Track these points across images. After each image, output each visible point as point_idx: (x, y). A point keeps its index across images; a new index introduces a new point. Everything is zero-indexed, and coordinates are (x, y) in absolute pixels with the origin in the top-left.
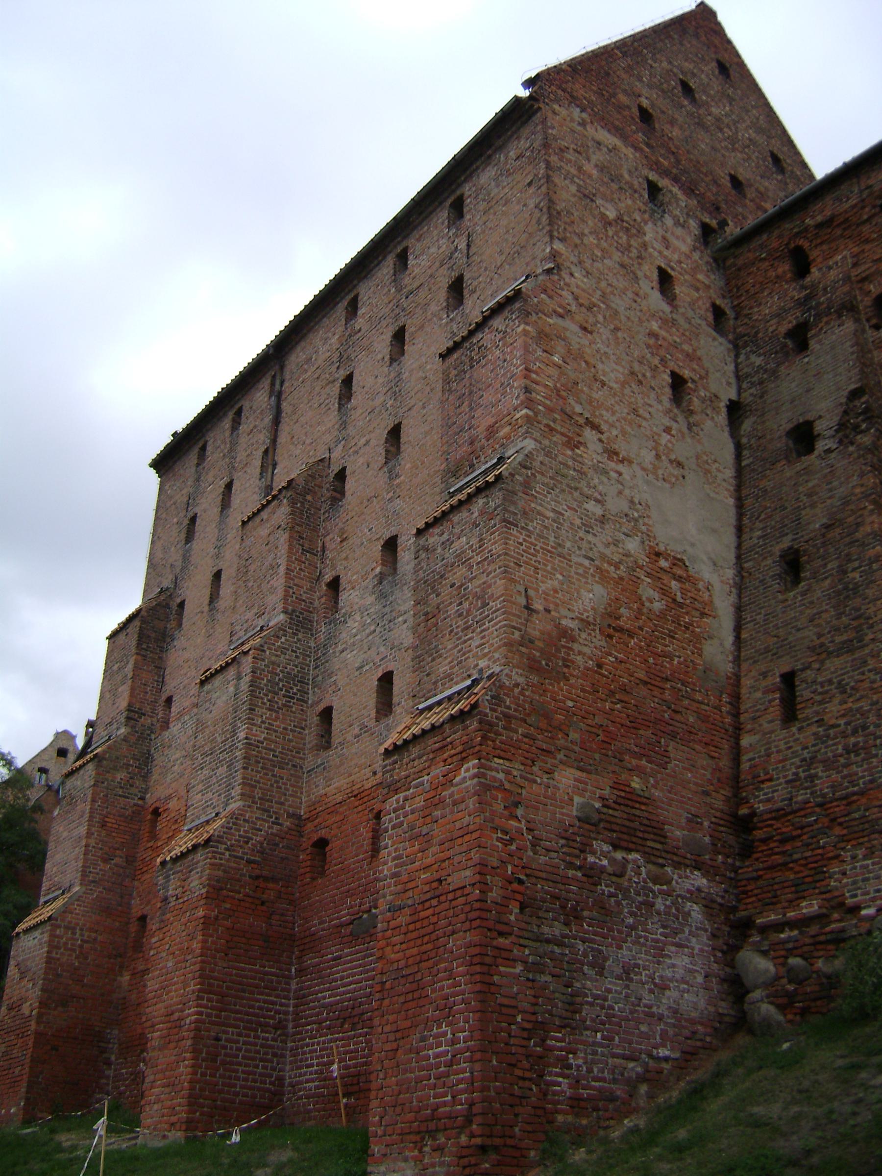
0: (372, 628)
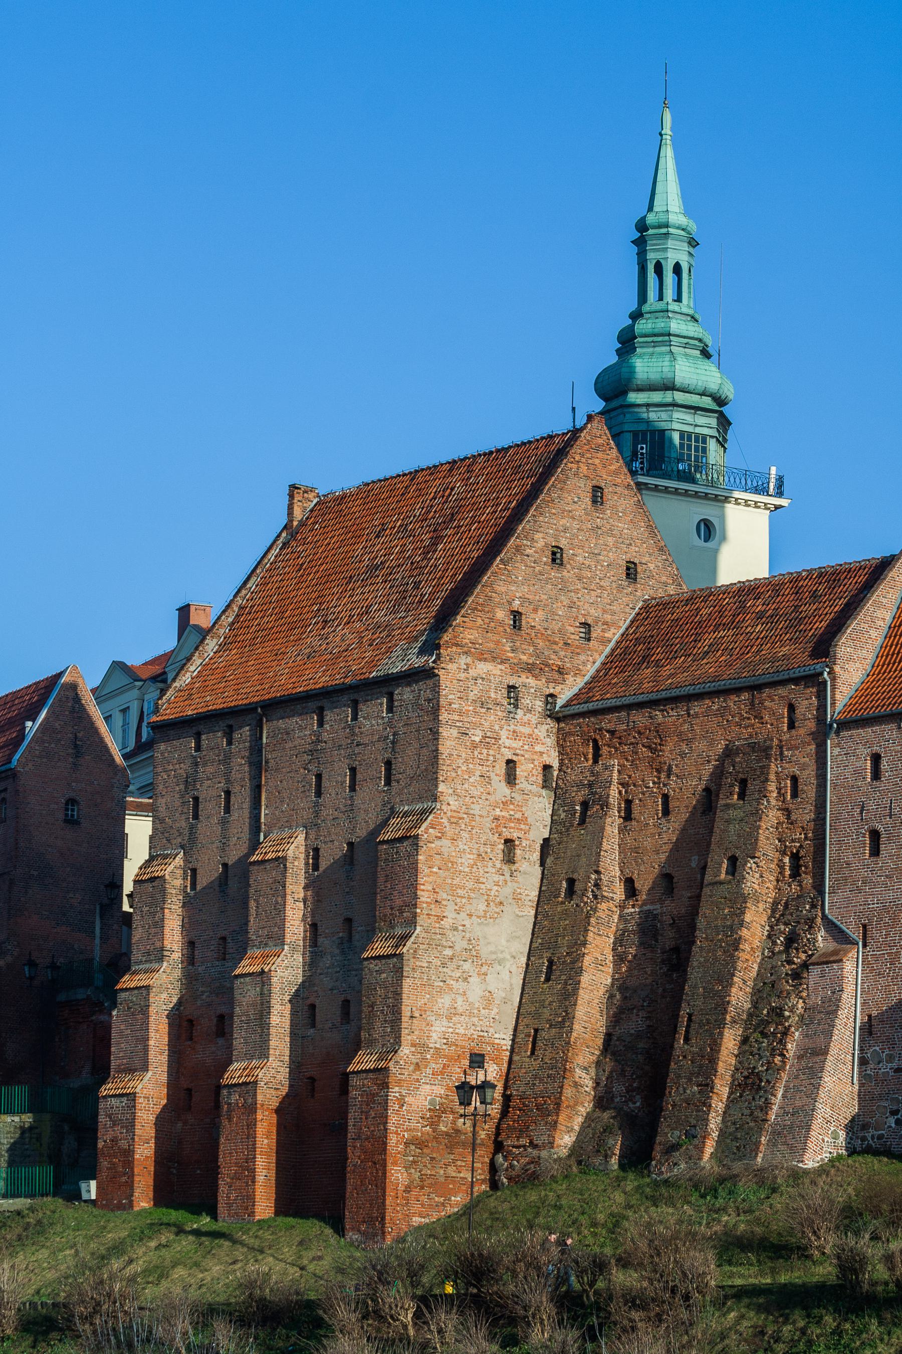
0: (338, 969)
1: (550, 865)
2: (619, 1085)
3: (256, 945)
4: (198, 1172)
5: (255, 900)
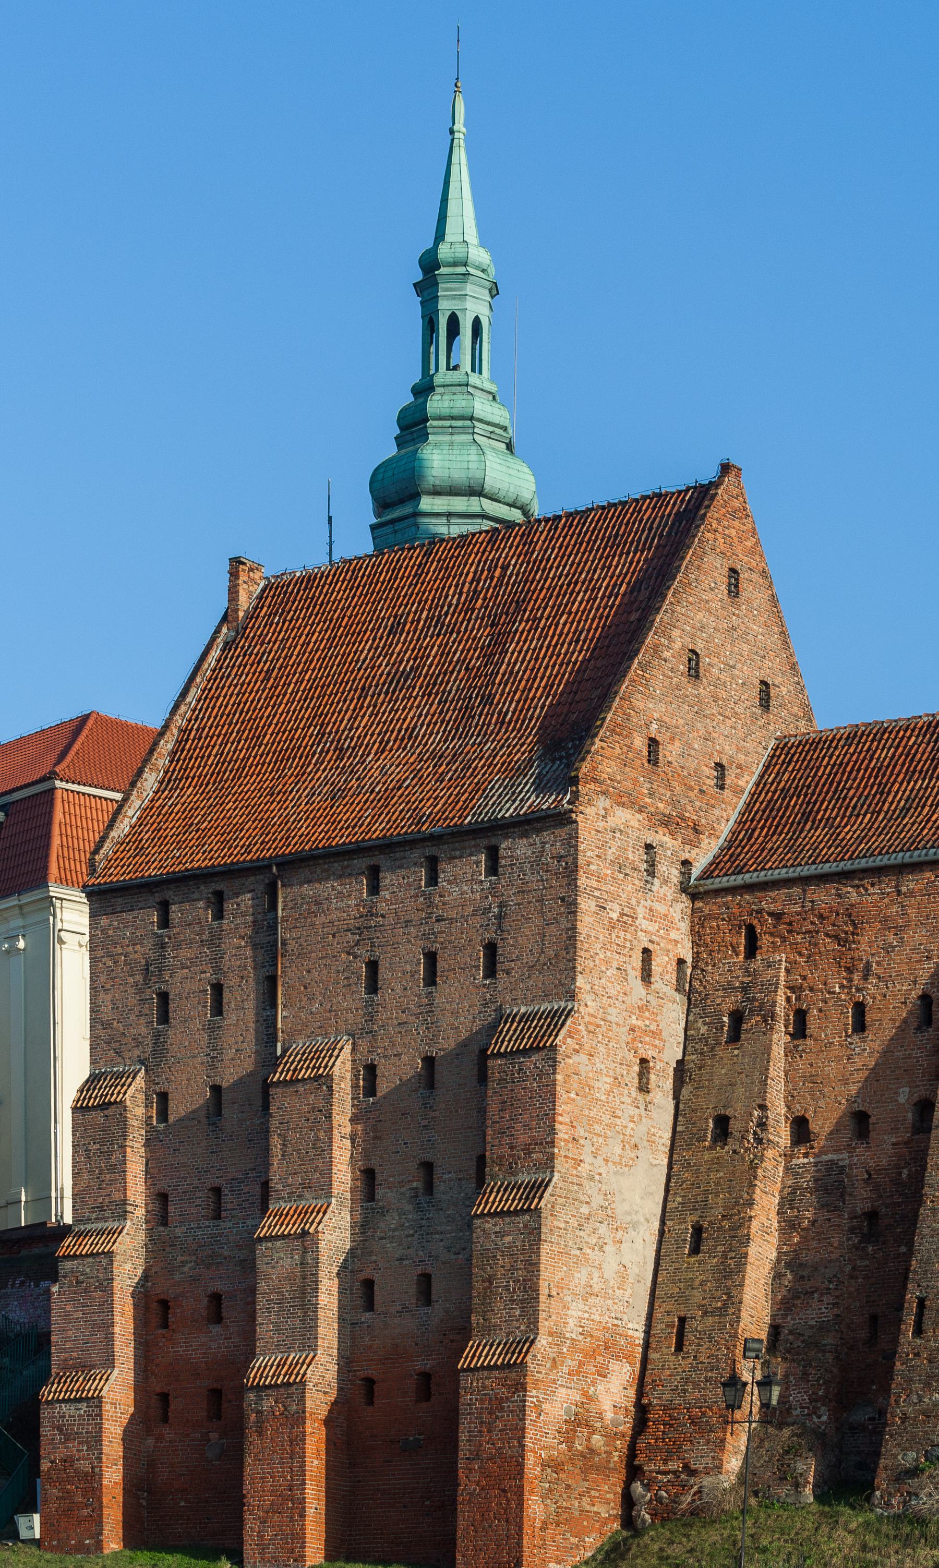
0: (411, 1232)
1: (687, 1097)
2: (799, 1393)
3: (283, 1198)
4: (183, 1504)
5: (279, 1134)
